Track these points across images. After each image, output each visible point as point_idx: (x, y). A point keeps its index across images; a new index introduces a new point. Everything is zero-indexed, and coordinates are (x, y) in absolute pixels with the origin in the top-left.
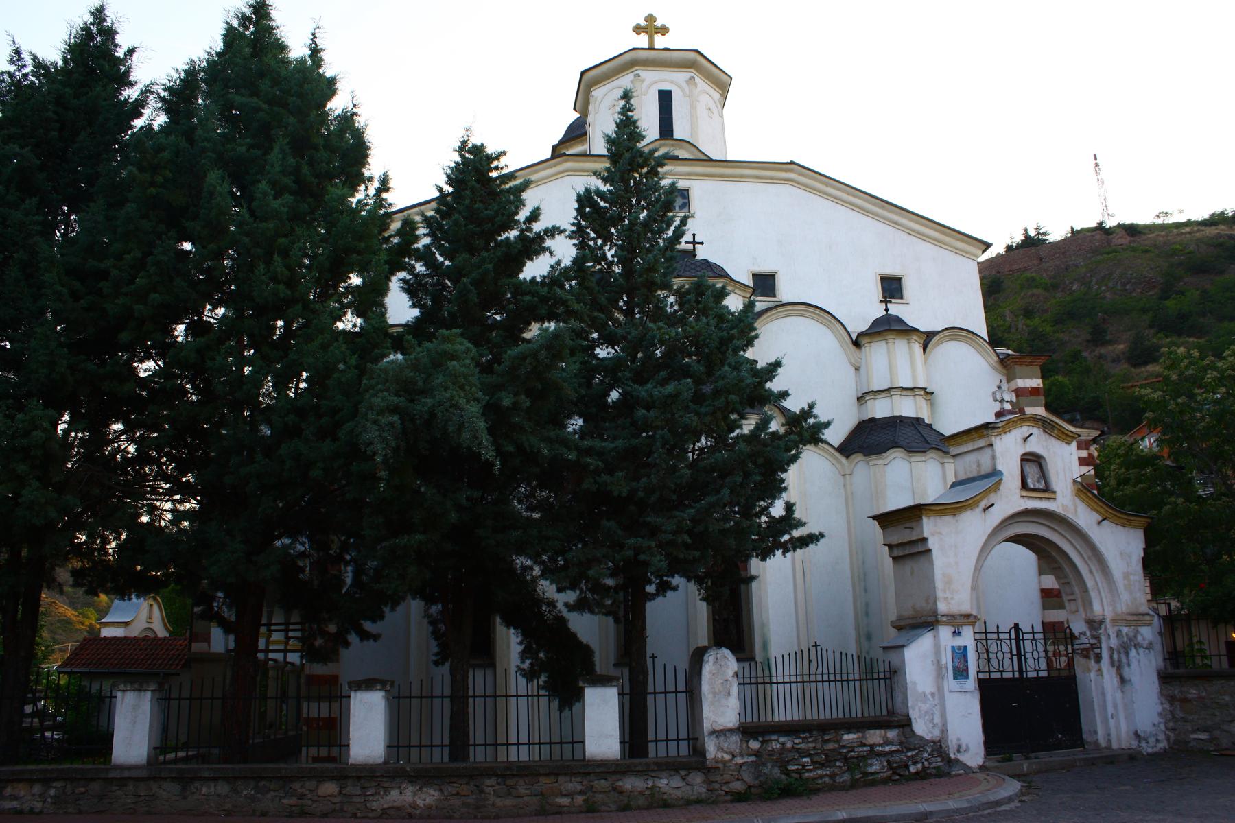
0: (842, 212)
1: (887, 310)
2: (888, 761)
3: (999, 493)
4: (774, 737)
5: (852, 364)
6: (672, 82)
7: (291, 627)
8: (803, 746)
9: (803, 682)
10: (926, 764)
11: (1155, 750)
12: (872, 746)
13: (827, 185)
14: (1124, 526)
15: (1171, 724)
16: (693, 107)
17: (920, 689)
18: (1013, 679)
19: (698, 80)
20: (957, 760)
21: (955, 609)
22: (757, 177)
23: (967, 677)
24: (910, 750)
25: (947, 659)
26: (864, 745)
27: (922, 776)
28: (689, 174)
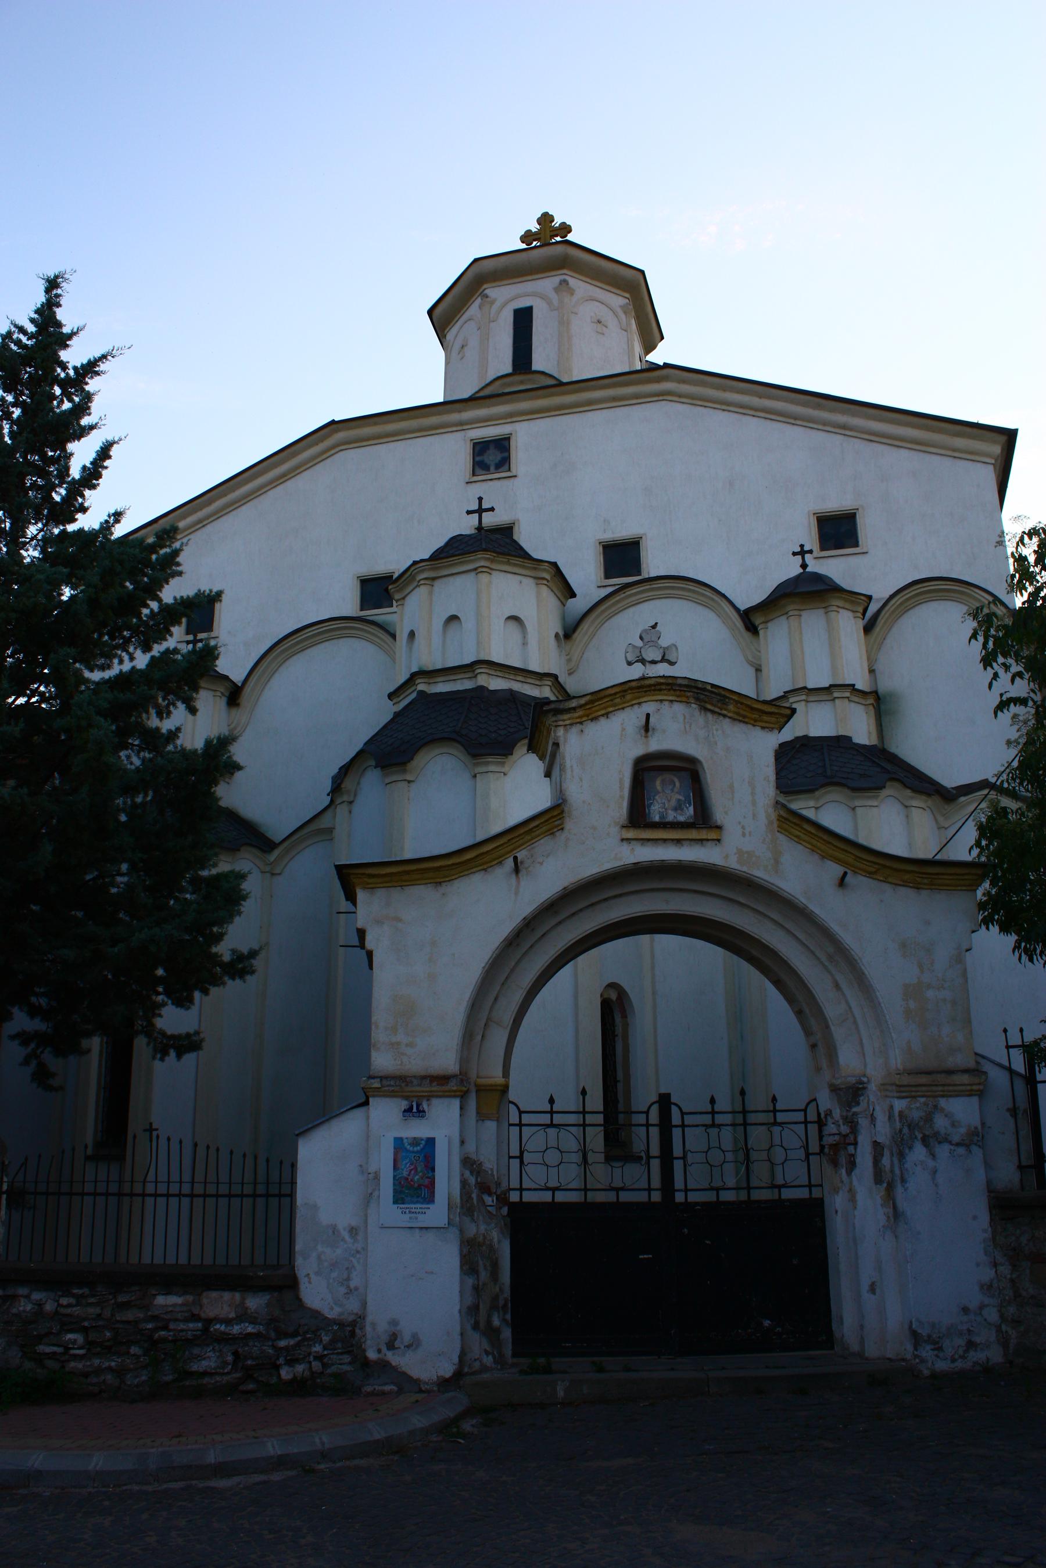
0: (753, 426)
1: (804, 566)
2: (236, 1354)
3: (561, 837)
4: (22, 1291)
5: (751, 663)
6: (534, 294)
7: (572, 1119)
8: (76, 1310)
9: (192, 1196)
10: (316, 1366)
11: (959, 1364)
12: (209, 1322)
13: (724, 389)
14: (917, 887)
15: (1012, 1310)
16: (564, 324)
17: (325, 1217)
18: (649, 1205)
19: (572, 282)
20: (384, 1365)
21: (414, 1063)
22: (615, 399)
23: (430, 1199)
24: (287, 1335)
25: (384, 1162)
26: (194, 1317)
27: (300, 1388)
28: (511, 415)
